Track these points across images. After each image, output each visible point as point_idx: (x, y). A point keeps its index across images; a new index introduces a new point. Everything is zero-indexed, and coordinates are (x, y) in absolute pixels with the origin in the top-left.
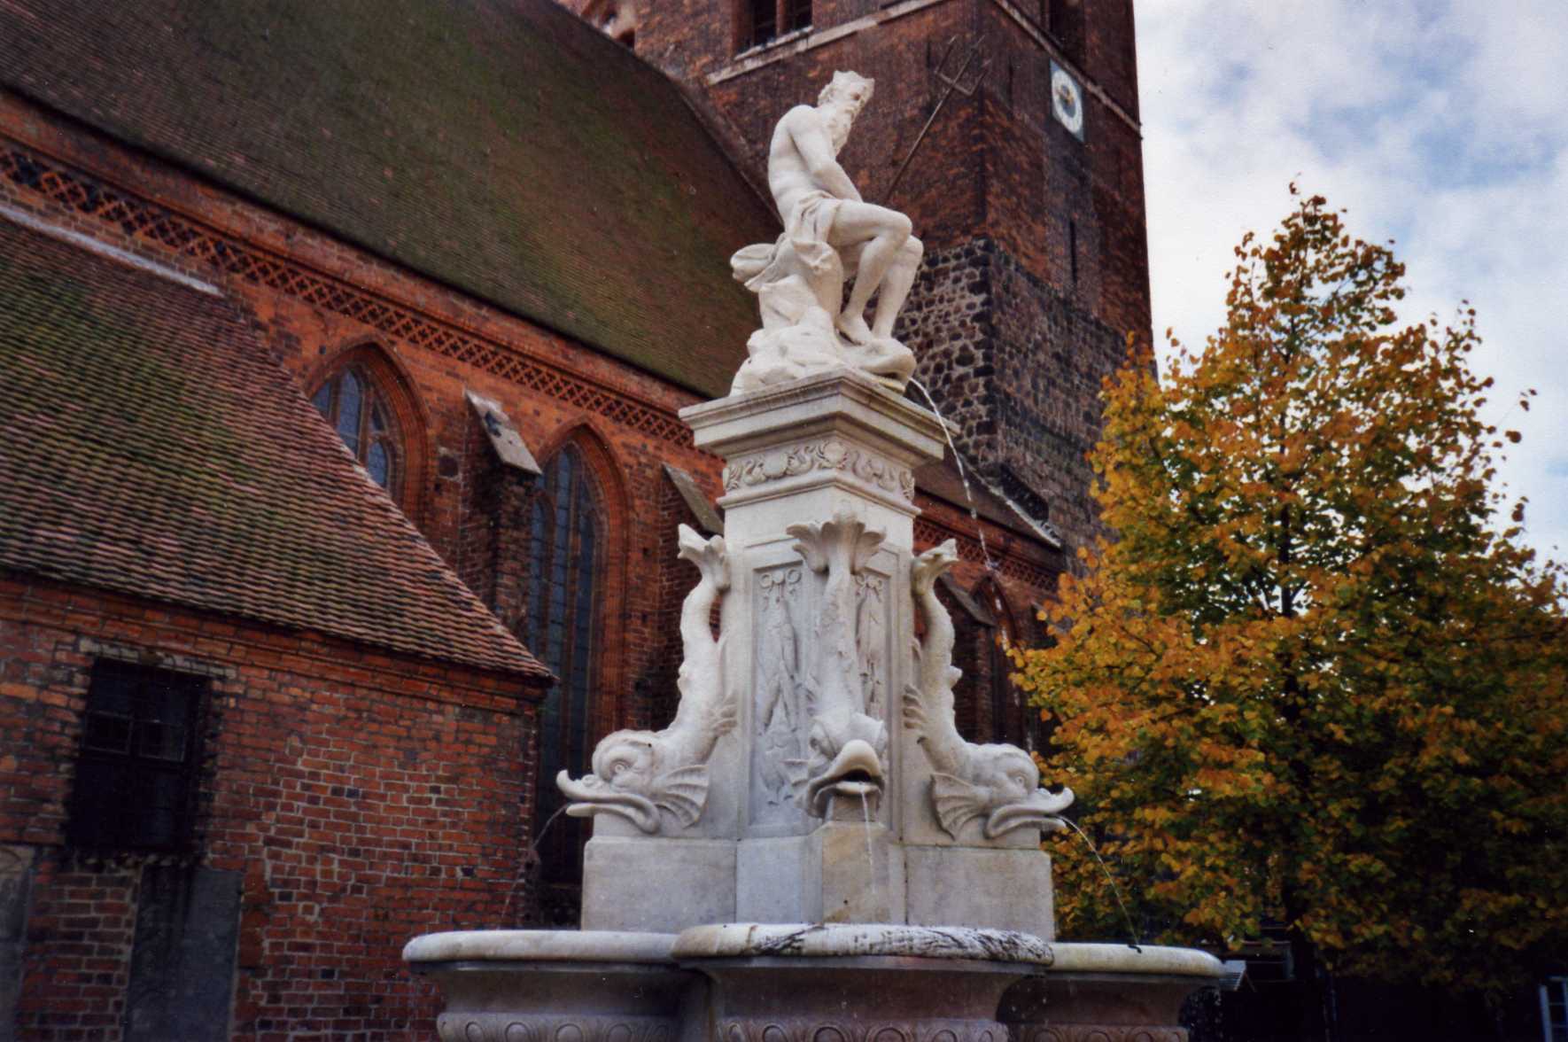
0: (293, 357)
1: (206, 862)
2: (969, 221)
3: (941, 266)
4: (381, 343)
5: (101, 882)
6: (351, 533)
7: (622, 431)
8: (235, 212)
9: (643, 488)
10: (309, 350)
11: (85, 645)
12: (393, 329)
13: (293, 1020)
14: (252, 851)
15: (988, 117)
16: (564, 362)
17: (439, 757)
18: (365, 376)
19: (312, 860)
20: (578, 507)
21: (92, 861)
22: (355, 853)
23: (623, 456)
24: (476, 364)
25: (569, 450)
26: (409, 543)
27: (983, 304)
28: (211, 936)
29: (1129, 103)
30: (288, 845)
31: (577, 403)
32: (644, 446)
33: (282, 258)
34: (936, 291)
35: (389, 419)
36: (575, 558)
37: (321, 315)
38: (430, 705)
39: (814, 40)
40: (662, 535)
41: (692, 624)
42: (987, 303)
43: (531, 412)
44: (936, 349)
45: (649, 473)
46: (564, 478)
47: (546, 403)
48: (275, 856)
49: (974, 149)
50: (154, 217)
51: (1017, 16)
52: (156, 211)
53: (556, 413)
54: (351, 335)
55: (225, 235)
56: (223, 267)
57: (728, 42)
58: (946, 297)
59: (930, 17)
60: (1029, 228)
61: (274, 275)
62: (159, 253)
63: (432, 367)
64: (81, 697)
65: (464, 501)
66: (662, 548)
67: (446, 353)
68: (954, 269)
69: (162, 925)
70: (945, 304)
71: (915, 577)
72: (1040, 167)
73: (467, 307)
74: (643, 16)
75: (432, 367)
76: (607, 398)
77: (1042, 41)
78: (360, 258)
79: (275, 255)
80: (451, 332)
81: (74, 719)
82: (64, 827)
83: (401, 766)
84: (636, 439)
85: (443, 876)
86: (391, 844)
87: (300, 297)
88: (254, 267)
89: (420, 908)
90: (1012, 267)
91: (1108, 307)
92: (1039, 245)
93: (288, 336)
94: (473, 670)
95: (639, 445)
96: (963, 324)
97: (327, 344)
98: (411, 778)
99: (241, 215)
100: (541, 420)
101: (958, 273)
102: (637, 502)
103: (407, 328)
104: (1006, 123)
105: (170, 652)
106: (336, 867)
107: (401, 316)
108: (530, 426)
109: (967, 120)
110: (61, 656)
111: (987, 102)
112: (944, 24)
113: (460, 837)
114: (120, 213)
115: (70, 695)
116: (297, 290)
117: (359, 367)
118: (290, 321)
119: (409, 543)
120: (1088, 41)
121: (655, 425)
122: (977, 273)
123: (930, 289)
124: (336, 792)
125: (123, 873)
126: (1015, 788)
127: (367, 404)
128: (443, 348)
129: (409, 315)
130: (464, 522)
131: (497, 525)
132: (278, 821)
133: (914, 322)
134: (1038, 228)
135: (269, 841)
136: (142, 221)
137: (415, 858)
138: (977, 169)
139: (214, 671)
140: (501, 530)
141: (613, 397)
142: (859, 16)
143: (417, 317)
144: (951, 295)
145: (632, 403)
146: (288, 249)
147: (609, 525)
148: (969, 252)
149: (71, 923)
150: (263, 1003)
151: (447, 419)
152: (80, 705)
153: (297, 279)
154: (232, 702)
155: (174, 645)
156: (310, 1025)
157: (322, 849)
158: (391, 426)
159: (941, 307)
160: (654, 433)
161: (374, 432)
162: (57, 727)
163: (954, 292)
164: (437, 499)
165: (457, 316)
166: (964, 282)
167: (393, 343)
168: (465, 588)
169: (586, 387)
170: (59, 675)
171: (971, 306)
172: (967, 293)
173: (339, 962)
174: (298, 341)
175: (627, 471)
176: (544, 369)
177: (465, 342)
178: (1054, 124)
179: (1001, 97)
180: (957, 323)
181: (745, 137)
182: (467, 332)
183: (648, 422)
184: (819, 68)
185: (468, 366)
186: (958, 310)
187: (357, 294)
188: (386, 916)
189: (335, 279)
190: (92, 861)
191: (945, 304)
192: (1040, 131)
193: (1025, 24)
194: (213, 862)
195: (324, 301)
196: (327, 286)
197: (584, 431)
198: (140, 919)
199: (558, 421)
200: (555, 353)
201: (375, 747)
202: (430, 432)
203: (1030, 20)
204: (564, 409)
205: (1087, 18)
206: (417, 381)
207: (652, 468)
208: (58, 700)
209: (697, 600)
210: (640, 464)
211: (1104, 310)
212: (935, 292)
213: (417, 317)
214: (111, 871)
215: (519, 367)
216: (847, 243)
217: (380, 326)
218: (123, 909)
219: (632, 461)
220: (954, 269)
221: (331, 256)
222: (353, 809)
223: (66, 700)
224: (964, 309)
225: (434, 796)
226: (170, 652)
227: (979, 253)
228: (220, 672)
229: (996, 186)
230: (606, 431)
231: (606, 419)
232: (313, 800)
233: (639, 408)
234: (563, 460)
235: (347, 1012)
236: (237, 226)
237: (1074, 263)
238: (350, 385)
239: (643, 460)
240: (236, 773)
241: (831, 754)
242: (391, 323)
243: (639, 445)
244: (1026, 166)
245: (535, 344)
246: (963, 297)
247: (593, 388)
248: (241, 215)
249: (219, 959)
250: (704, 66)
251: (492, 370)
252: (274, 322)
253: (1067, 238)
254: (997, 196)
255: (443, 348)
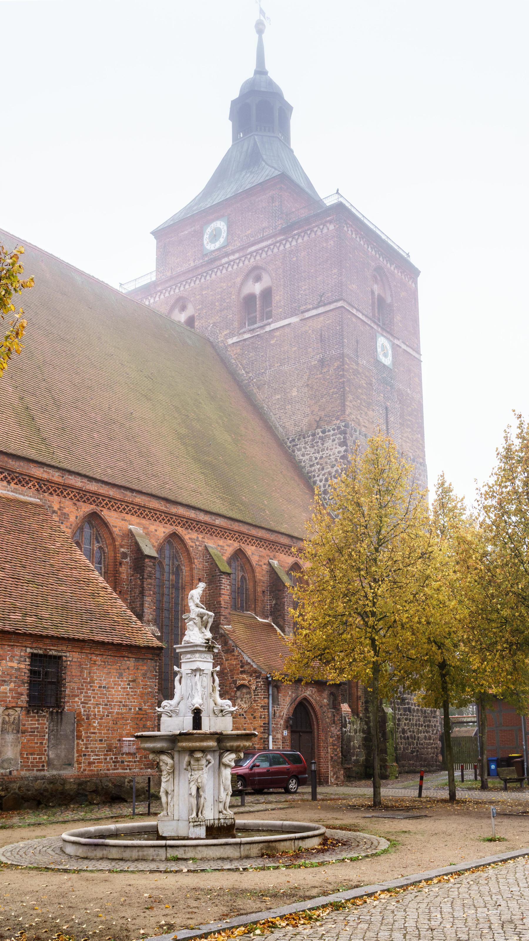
0: (67, 522)
1: (65, 710)
2: (339, 414)
3: (327, 433)
4: (97, 512)
5: (38, 716)
6: (96, 600)
7: (189, 533)
8: (44, 471)
9: (198, 555)
10: (72, 519)
11: (29, 650)
12: (102, 505)
13: (92, 754)
14: (78, 706)
15: (346, 366)
16: (166, 509)
17: (129, 674)
18: (92, 524)
19: (94, 708)
20: (173, 564)
21: (35, 711)
22: (106, 705)
23: (189, 543)
24: (132, 514)
25: (169, 542)
26: (115, 601)
27: (344, 451)
28: (68, 731)
29: (416, 345)
30: (87, 704)
31: (171, 525)
32: (198, 538)
33: (61, 485)
34: (326, 445)
35: (101, 539)
36: (173, 585)
37: (75, 504)
38: (125, 659)
39: (273, 326)
40: (206, 573)
41: (177, 683)
42: (346, 451)
43: (154, 530)
44: (325, 471)
45: (200, 548)
46: (167, 553)
47: (159, 526)
48: (84, 707)
49: (340, 381)
50: (17, 477)
51: (360, 315)
52: (17, 475)
53: (163, 530)
54: (87, 510)
55: (41, 480)
56: (41, 492)
57: (236, 324)
58: (329, 448)
59: (321, 318)
60: (366, 413)
61: (58, 492)
62: (19, 490)
63: (116, 518)
64: (29, 665)
65: (130, 568)
66: (206, 578)
67: (121, 512)
68: (332, 435)
69: (55, 728)
70: (329, 451)
71: (212, 673)
72: (371, 384)
73: (129, 493)
74: (199, 310)
75: (116, 518)
76: (182, 521)
77: (372, 325)
78: (88, 481)
79: (58, 484)
80: (122, 503)
81: (27, 672)
82: (28, 702)
83: (118, 678)
84: (194, 535)
85: (133, 710)
86: (116, 702)
87: (68, 498)
88: (51, 490)
89: (126, 720)
90: (358, 433)
91: (403, 443)
92: (371, 420)
93: (65, 514)
94: (138, 647)
95: (196, 538)
96: (336, 460)
97: (78, 515)
98: (121, 681)
99: (46, 472)
100: (157, 533)
101: (334, 437)
102: (196, 561)
103: (107, 504)
104: (355, 367)
105: (50, 650)
106: (101, 709)
107: (104, 500)
108: (153, 536)
109: (337, 367)
110: (22, 654)
111: (346, 359)
112: (327, 322)
113: (137, 698)
114: (5, 477)
115: (26, 665)
116: (66, 496)
117: (90, 521)
118: (65, 508)
119: (115, 601)
120: (395, 320)
121: (202, 529)
122: (342, 437)
123: (323, 444)
124: (100, 687)
125: (44, 714)
126: (227, 707)
127: (93, 534)
128: (120, 510)
129: (107, 499)
130: (131, 576)
131: (143, 578)
132: (84, 697)
133: (316, 458)
134: (370, 413)
135: (82, 703)
136: (13, 479)
137: (124, 706)
138: (342, 390)
139: (63, 654)
140: (145, 580)
141: (185, 520)
142: (292, 316)
143: (110, 500)
144: (331, 447)
145: (192, 522)
146: (63, 482)
147: (185, 570)
148: (339, 428)
149: (31, 728)
150: (84, 749)
151: (123, 537)
152: (29, 667)
153: (67, 492)
154: (69, 663)
155: (52, 648)
156: (97, 755)
157: (97, 704)
158: (102, 542)
159: (327, 452)
160: (201, 532)
161: (97, 545)
162: (23, 674)
163: (333, 445)
164: (120, 569)
165: (125, 497)
166: (337, 441)
167: (102, 511)
168: (134, 616)
169: (174, 517)
170: (22, 659)
171: (339, 452)
172: (338, 447)
173: (104, 737)
174: (68, 515)
175: (191, 549)
176: (158, 513)
177: (128, 506)
178: (378, 362)
179: (352, 355)
180: (334, 460)
181: (244, 370)
182: (129, 503)
183: (199, 528)
184: (275, 339)
185: (129, 515)
186: (334, 454)
187: (88, 494)
188: (116, 723)
189: (80, 490)
190: (35, 711)
191: (329, 451)
192: (371, 368)
193: (364, 318)
194: (68, 710)
195: (76, 499)
196: (77, 493)
197: (174, 535)
198: (49, 727)
199: (164, 532)
200: (162, 506)
201: (110, 673)
202: (117, 543)
203: (366, 316)
204: (166, 528)
205: (395, 308)
206: (111, 524)
207: (201, 546)
208: (23, 666)
209: (177, 678)
210: (196, 545)
211: (401, 445)
212: (325, 445)
213: (110, 500)
214: (41, 713)
215: (148, 513)
216: (201, 616)
217: (97, 505)
218: (45, 724)
219: (193, 544)
220: (332, 435)
221: (78, 482)
222: (105, 692)
223: (25, 666)
224: (337, 453)
225: (129, 687)
226: (50, 650)
227: (343, 428)
228: (65, 654)
229: (350, 397)
230: (183, 534)
231: (182, 529)
232: (94, 690)
233: (195, 523)
234: (167, 547)
235: (107, 751)
236: (45, 476)
237: (387, 426)
238: (87, 530)
239: (197, 543)
240: (71, 684)
241: (194, 706)
242: (100, 503)
243: (196, 538)
244: (364, 385)
245: (154, 504)
246: (336, 448)
247: (177, 518)
248: (46, 472)
249: (71, 737)
250: (226, 335)
251: (138, 516)
252: (59, 509)
253: (384, 415)
254: (351, 402)
255: (120, 510)
